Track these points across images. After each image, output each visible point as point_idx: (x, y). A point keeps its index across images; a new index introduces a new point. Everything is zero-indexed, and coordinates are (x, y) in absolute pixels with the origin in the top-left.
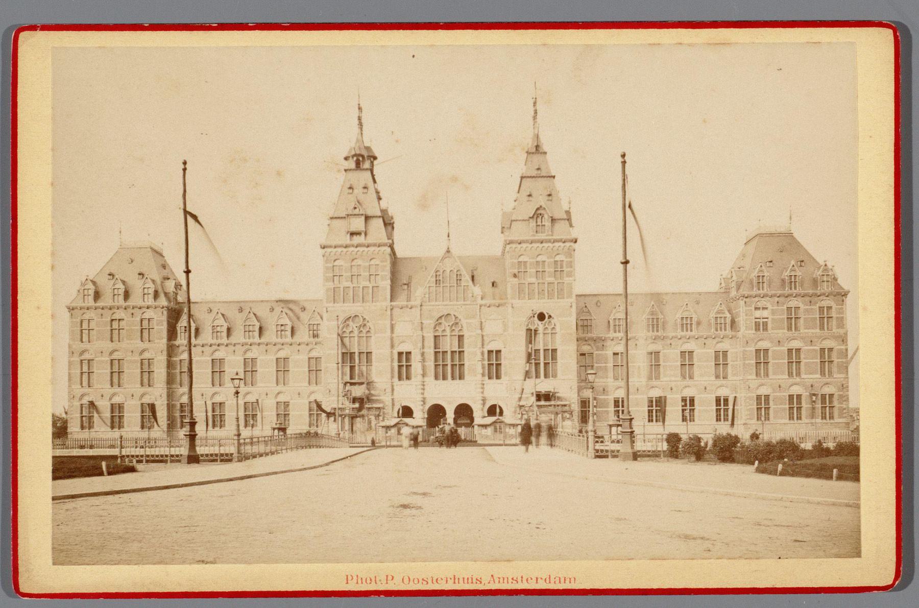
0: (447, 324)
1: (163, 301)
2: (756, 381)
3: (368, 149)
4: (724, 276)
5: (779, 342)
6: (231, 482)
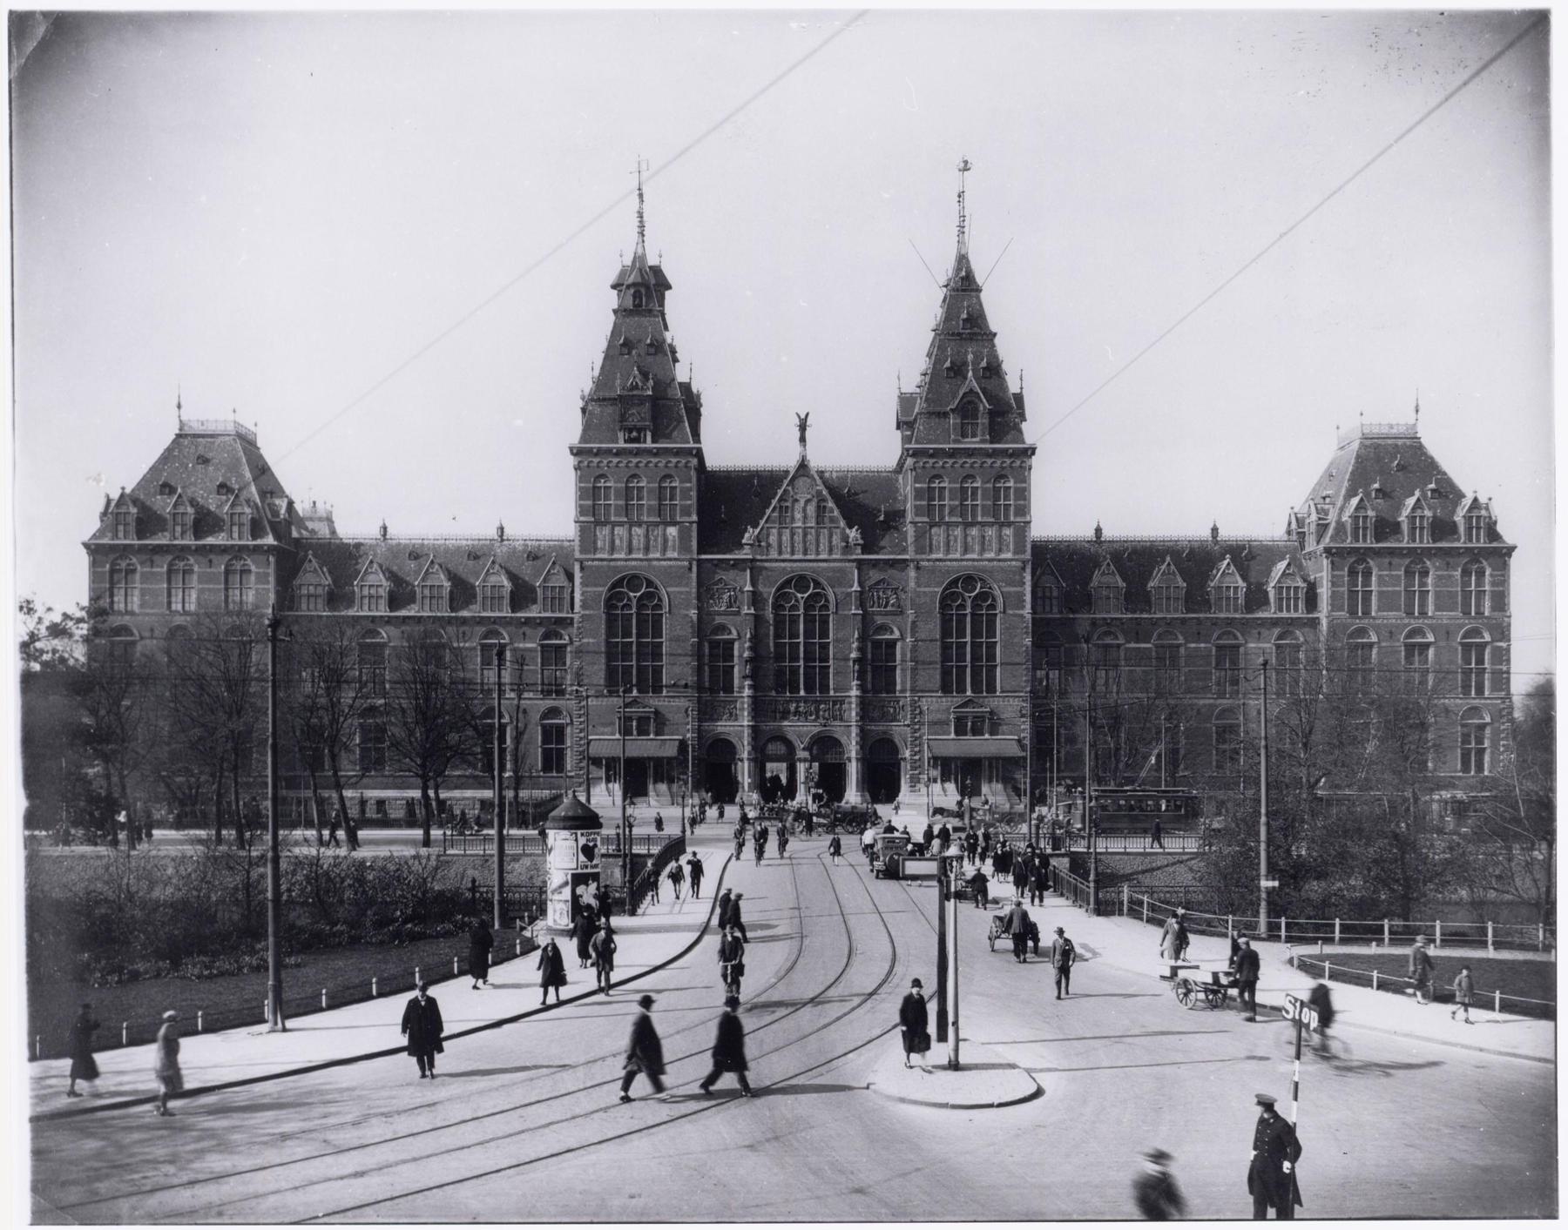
0: (799, 595)
1: (270, 540)
2: (944, 700)
3: (657, 271)
4: (1296, 510)
5: (1391, 632)
6: (573, 1153)
